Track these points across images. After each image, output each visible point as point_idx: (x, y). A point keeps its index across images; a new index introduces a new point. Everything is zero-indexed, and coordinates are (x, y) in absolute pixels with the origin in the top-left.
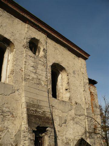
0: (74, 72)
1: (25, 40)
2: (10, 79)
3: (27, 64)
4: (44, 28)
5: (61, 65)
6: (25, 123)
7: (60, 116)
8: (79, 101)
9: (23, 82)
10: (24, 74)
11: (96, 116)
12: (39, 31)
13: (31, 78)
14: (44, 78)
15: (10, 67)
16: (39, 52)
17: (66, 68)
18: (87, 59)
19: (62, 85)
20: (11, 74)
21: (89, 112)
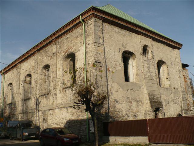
0: (172, 64)
1: (140, 49)
2: (136, 79)
3: (144, 66)
4: (150, 35)
5: (163, 61)
6: (149, 106)
7: (165, 99)
8: (176, 86)
9: (144, 80)
10: (144, 75)
11: (188, 95)
12: (147, 37)
13: (147, 76)
14: (154, 75)
15: (135, 71)
16: (148, 54)
17: (166, 62)
18: (181, 48)
19: (163, 75)
20: (136, 76)
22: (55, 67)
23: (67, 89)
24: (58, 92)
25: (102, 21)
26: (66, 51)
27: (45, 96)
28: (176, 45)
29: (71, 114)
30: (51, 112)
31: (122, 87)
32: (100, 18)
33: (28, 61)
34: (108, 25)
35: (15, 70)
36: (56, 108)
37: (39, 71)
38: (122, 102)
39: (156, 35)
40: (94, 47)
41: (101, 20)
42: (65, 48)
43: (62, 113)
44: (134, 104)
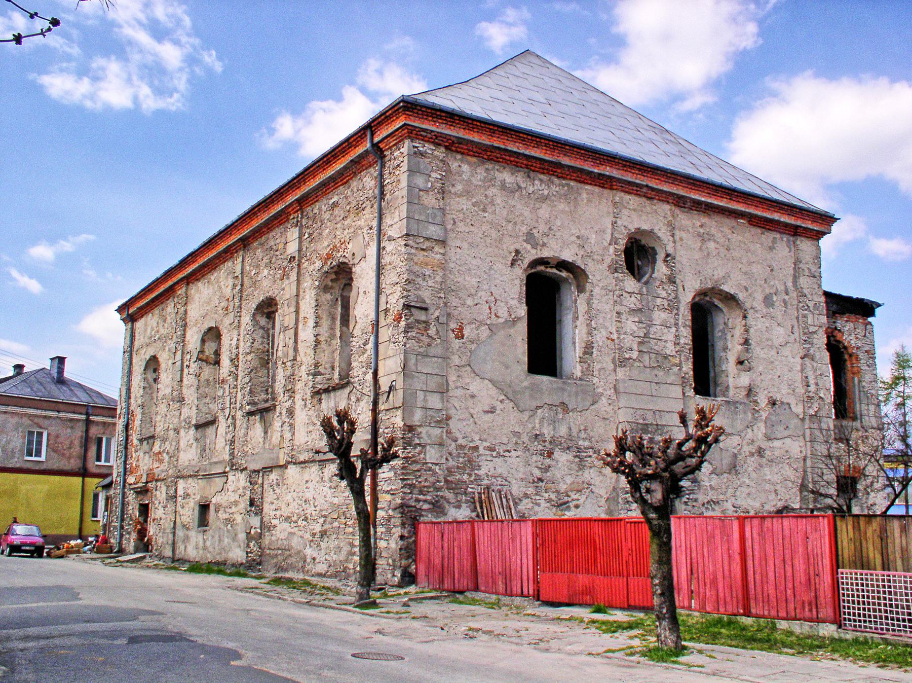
8: (782, 394)
18: (824, 234)
20: (585, 353)
22: (293, 309)
23: (323, 396)
24: (299, 403)
25: (443, 149)
26: (329, 256)
27: (258, 417)
28: (799, 223)
29: (330, 488)
30: (273, 476)
31: (510, 394)
32: (437, 140)
33: (213, 277)
34: (469, 164)
35: (170, 308)
36: (289, 463)
37: (246, 319)
38: (508, 451)
39: (694, 185)
40: (403, 249)
41: (440, 145)
42: (326, 243)
43: (307, 482)
44: (563, 458)
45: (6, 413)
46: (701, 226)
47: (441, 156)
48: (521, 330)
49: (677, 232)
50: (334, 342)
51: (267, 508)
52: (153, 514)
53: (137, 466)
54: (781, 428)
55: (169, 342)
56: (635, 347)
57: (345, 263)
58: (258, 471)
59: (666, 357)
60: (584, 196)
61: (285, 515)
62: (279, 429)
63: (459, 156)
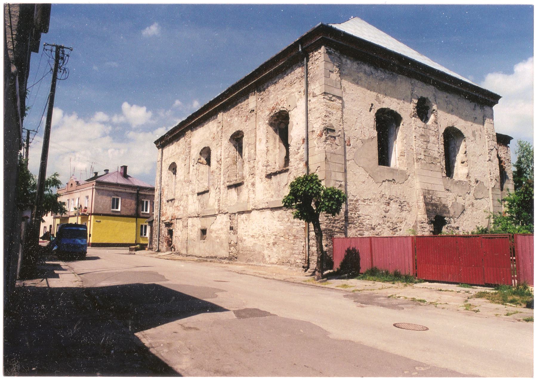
6: (423, 213)
9: (415, 163)
21: (496, 192)
36: (253, 209)
44: (394, 206)
45: (103, 190)
46: (447, 97)
47: (338, 55)
48: (375, 143)
49: (437, 100)
50: (276, 150)
51: (240, 231)
52: (174, 234)
53: (166, 213)
54: (480, 193)
55: (182, 155)
56: (423, 153)
57: (285, 111)
58: (235, 214)
59: (435, 158)
60: (399, 79)
61: (251, 235)
62: (247, 193)
63: (345, 56)
